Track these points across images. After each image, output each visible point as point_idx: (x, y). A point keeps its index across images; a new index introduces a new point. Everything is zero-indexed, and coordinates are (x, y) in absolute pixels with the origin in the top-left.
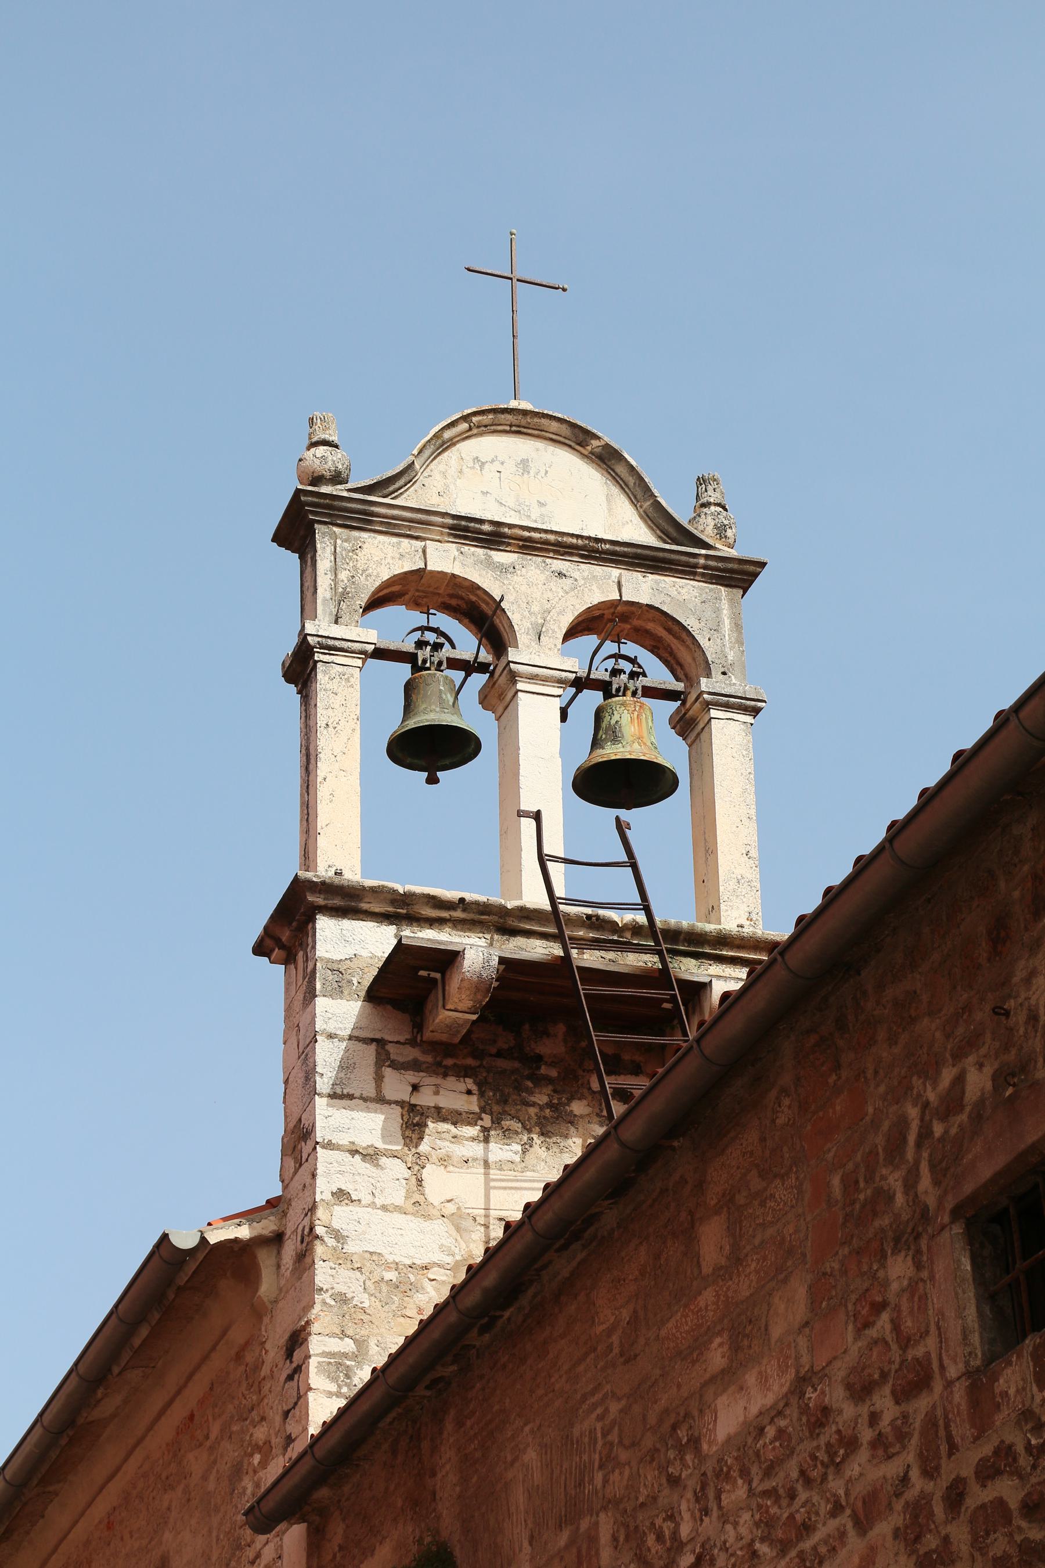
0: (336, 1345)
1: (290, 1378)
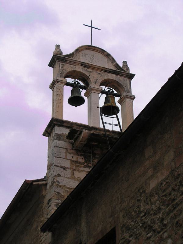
1: (49, 208)
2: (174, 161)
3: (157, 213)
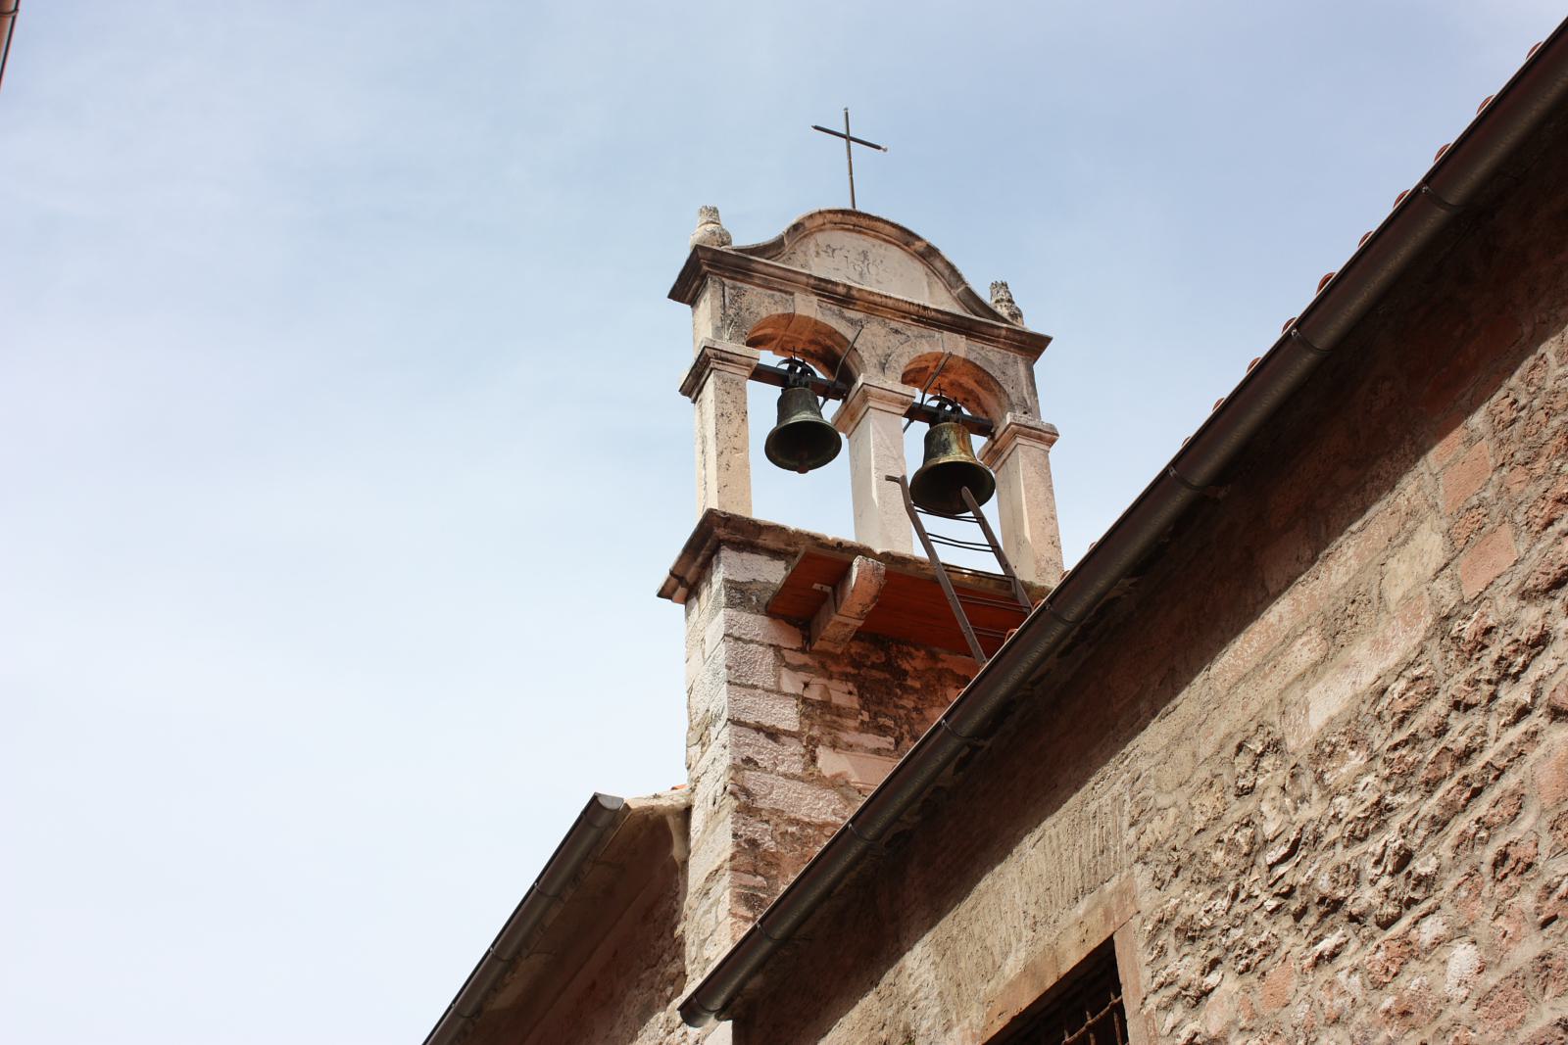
2: (1447, 571)
3: (1367, 834)
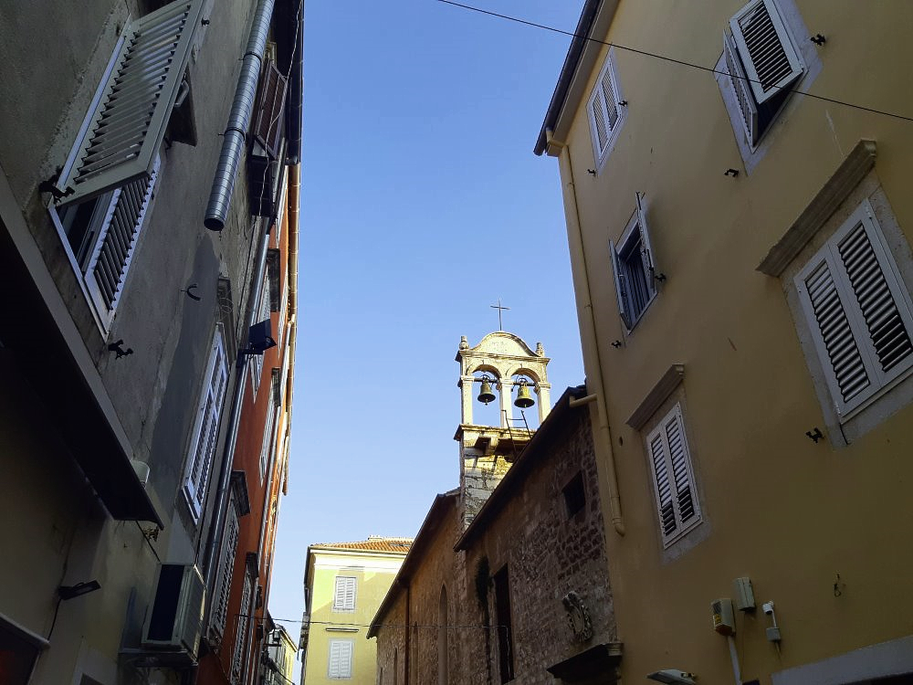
0: (469, 516)
